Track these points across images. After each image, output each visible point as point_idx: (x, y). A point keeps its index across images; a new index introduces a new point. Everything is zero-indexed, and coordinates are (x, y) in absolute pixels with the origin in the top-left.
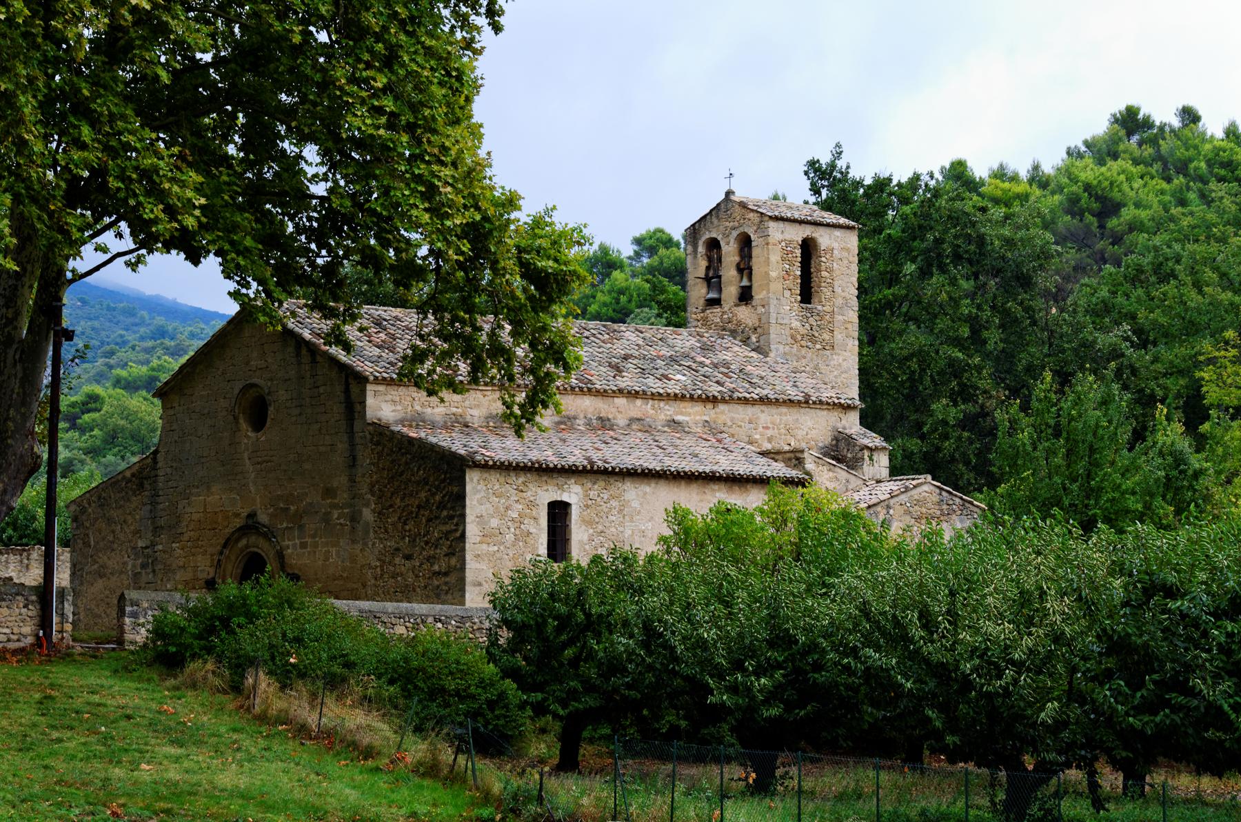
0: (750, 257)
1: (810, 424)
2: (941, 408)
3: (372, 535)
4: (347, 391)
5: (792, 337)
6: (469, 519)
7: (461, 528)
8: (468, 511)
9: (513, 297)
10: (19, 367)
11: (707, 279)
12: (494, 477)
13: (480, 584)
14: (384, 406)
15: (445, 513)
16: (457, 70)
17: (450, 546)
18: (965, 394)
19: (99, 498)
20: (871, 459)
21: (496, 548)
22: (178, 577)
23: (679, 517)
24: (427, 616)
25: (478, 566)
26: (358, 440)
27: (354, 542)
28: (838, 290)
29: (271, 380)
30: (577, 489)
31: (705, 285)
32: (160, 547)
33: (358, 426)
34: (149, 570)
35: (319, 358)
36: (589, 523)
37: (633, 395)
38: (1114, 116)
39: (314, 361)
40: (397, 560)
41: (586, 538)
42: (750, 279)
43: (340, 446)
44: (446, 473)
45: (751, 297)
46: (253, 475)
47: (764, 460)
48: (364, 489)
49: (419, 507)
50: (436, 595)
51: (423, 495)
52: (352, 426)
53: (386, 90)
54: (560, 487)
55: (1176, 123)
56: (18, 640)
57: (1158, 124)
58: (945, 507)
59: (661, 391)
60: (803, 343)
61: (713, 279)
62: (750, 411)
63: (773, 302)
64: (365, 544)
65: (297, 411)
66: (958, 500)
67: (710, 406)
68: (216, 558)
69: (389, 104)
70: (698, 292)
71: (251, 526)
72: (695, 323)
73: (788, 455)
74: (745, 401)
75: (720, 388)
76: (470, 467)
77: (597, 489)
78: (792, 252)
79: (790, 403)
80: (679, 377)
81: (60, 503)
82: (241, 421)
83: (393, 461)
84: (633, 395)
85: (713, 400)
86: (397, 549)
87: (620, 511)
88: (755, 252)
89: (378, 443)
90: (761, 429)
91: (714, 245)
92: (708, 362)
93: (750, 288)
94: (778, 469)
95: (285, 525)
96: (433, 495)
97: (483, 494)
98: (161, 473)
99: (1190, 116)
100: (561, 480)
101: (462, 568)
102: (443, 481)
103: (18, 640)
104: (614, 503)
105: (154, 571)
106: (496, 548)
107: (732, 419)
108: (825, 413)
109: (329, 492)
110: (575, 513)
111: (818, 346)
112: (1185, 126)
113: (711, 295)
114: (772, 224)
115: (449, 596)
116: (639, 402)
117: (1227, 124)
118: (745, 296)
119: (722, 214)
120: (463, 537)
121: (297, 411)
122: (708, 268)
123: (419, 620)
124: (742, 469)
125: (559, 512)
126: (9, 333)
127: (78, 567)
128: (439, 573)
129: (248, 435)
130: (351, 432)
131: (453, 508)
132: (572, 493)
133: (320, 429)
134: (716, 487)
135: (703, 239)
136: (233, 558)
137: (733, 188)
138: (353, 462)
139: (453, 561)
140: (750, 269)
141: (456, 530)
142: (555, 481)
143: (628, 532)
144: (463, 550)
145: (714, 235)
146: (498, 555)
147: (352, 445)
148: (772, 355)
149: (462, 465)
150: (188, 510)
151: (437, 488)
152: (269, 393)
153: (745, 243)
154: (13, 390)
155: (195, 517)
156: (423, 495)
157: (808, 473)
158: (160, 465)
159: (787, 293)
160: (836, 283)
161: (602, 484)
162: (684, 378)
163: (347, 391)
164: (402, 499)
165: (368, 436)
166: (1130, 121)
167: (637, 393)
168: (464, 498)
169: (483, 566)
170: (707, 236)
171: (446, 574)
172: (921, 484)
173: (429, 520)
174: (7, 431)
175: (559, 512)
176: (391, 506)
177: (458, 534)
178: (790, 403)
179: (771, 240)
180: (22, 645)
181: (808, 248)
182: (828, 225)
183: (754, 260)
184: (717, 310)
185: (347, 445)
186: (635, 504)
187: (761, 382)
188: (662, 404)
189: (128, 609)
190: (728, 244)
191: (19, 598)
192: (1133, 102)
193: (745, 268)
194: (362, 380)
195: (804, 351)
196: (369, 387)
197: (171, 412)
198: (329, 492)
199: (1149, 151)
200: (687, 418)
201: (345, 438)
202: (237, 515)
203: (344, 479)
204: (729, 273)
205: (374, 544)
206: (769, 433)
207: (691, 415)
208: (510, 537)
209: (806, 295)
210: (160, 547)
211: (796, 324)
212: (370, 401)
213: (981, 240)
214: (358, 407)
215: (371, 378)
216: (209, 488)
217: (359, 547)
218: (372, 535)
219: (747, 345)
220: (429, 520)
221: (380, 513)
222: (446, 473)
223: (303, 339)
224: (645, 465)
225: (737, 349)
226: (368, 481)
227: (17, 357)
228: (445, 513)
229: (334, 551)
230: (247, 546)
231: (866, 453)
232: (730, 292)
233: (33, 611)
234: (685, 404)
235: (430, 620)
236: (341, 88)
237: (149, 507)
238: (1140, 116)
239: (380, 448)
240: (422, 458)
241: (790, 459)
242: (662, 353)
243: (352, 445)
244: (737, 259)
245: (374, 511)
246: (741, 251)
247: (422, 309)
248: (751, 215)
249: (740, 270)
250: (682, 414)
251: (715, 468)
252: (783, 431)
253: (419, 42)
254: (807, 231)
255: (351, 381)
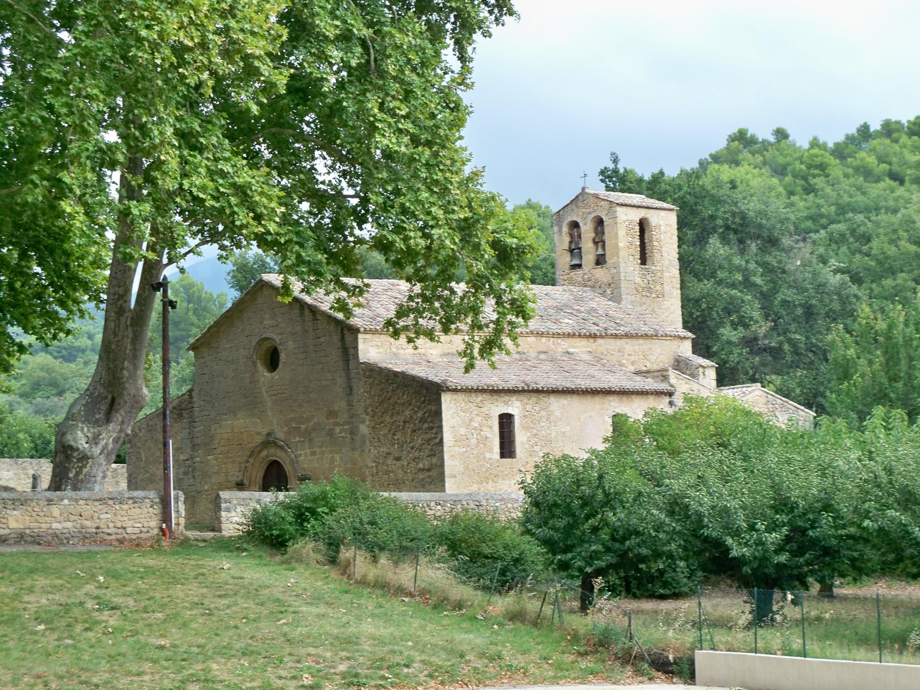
0: (603, 233)
2: (728, 333)
3: (368, 443)
4: (343, 339)
5: (636, 289)
6: (445, 429)
7: (439, 436)
8: (444, 423)
9: (479, 265)
10: (130, 330)
11: (571, 251)
12: (460, 397)
13: (455, 477)
14: (371, 349)
15: (426, 425)
16: (454, 102)
17: (432, 450)
18: (743, 322)
19: (148, 425)
20: (704, 375)
21: (464, 450)
22: (213, 481)
23: (619, 422)
24: (430, 501)
25: (453, 463)
26: (353, 375)
27: (353, 449)
28: (665, 254)
29: (281, 334)
30: (517, 404)
31: (569, 254)
32: (198, 459)
33: (352, 364)
34: (190, 476)
35: (319, 317)
36: (526, 428)
37: (540, 334)
38: (730, 136)
39: (315, 319)
40: (389, 462)
41: (525, 439)
42: (604, 248)
43: (339, 380)
44: (425, 396)
45: (605, 262)
46: (270, 404)
47: (638, 378)
48: (360, 410)
49: (405, 422)
50: (422, 486)
51: (407, 413)
52: (348, 365)
53: (406, 117)
54: (506, 403)
55: (772, 139)
56: (148, 532)
57: (760, 140)
58: (771, 406)
59: (559, 331)
60: (644, 293)
61: (575, 250)
63: (622, 265)
64: (363, 451)
65: (303, 356)
66: (779, 401)
67: (591, 340)
68: (243, 465)
69: (409, 126)
70: (564, 260)
71: (269, 442)
72: (563, 282)
73: (656, 374)
74: (616, 336)
75: (597, 328)
76: (444, 391)
77: (531, 402)
78: (633, 229)
79: (646, 336)
80: (567, 321)
82: (259, 365)
83: (382, 389)
84: (540, 334)
85: (594, 336)
86: (389, 454)
87: (548, 419)
88: (606, 230)
89: (369, 377)
91: (575, 225)
92: (582, 309)
93: (604, 255)
94: (650, 384)
95: (297, 439)
96: (416, 412)
97: (454, 410)
98: (196, 405)
99: (781, 134)
100: (506, 398)
101: (442, 465)
102: (424, 402)
103: (148, 532)
104: (543, 413)
105: (194, 477)
106: (464, 450)
107: (607, 350)
108: (668, 342)
109: (332, 414)
110: (517, 421)
111: (654, 295)
112: (779, 141)
113: (574, 262)
114: (619, 209)
115: (432, 486)
116: (544, 340)
117: (811, 139)
118: (600, 261)
119: (580, 204)
120: (441, 442)
121: (303, 356)
122: (571, 242)
123: (425, 505)
124: (628, 385)
125: (506, 421)
126: (121, 306)
127: (133, 476)
128: (423, 470)
129: (264, 375)
130: (347, 370)
131: (432, 422)
132: (514, 407)
133: (322, 369)
135: (566, 222)
136: (257, 465)
137: (587, 185)
138: (350, 390)
139: (434, 460)
140: (604, 242)
141: (436, 438)
142: (502, 399)
143: (554, 434)
144: (442, 451)
145: (575, 219)
146: (466, 454)
147: (349, 379)
148: (623, 302)
149: (437, 391)
150: (219, 431)
151: (419, 407)
152: (280, 344)
153: (599, 223)
154: (126, 348)
155: (225, 436)
156: (407, 413)
157: (672, 386)
158: (195, 399)
159: (631, 258)
160: (664, 250)
161: (534, 399)
162: (571, 322)
163: (343, 339)
164: (391, 417)
165: (362, 372)
166: (742, 138)
167: (543, 333)
168: (441, 414)
169: (457, 463)
170: (570, 219)
171: (429, 470)
172: (754, 390)
173: (414, 431)
174: (122, 378)
175: (506, 421)
176: (382, 422)
177: (437, 440)
178: (646, 336)
179: (619, 220)
180: (150, 534)
181: (643, 225)
182: (656, 209)
183: (606, 235)
184: (579, 272)
185: (344, 379)
186: (558, 414)
187: (623, 323)
188: (559, 341)
189: (223, 505)
190: (585, 224)
191: (147, 500)
192: (743, 126)
193: (599, 241)
194: (355, 331)
195: (644, 299)
196: (360, 336)
197: (202, 361)
198: (332, 414)
199: (759, 159)
200: (577, 350)
201: (343, 373)
202: (259, 434)
203: (343, 404)
204: (587, 245)
205: (370, 450)
206: (632, 358)
207: (580, 347)
208: (474, 441)
209: (644, 260)
210: (198, 459)
211: (638, 280)
212: (361, 346)
213: (743, 216)
214: (352, 351)
215: (362, 330)
216: (235, 415)
217: (357, 453)
218: (368, 443)
219: (604, 296)
220: (414, 431)
221: (373, 428)
222: (425, 396)
223: (306, 303)
224: (564, 384)
225: (598, 299)
226: (363, 404)
227: (129, 322)
228: (426, 425)
229: (337, 457)
230: (268, 456)
231: (701, 370)
232: (589, 257)
233: (157, 509)
235: (433, 504)
236: (374, 116)
237: (187, 431)
238: (749, 135)
239: (371, 380)
240: (406, 386)
241: (658, 376)
242: (550, 304)
243: (349, 379)
244: (593, 235)
245: (368, 426)
246: (596, 229)
247: (409, 280)
248: (603, 203)
249: (595, 243)
250: (573, 347)
251: (610, 385)
252: (641, 357)
253: (427, 81)
254: (642, 213)
255: (345, 332)
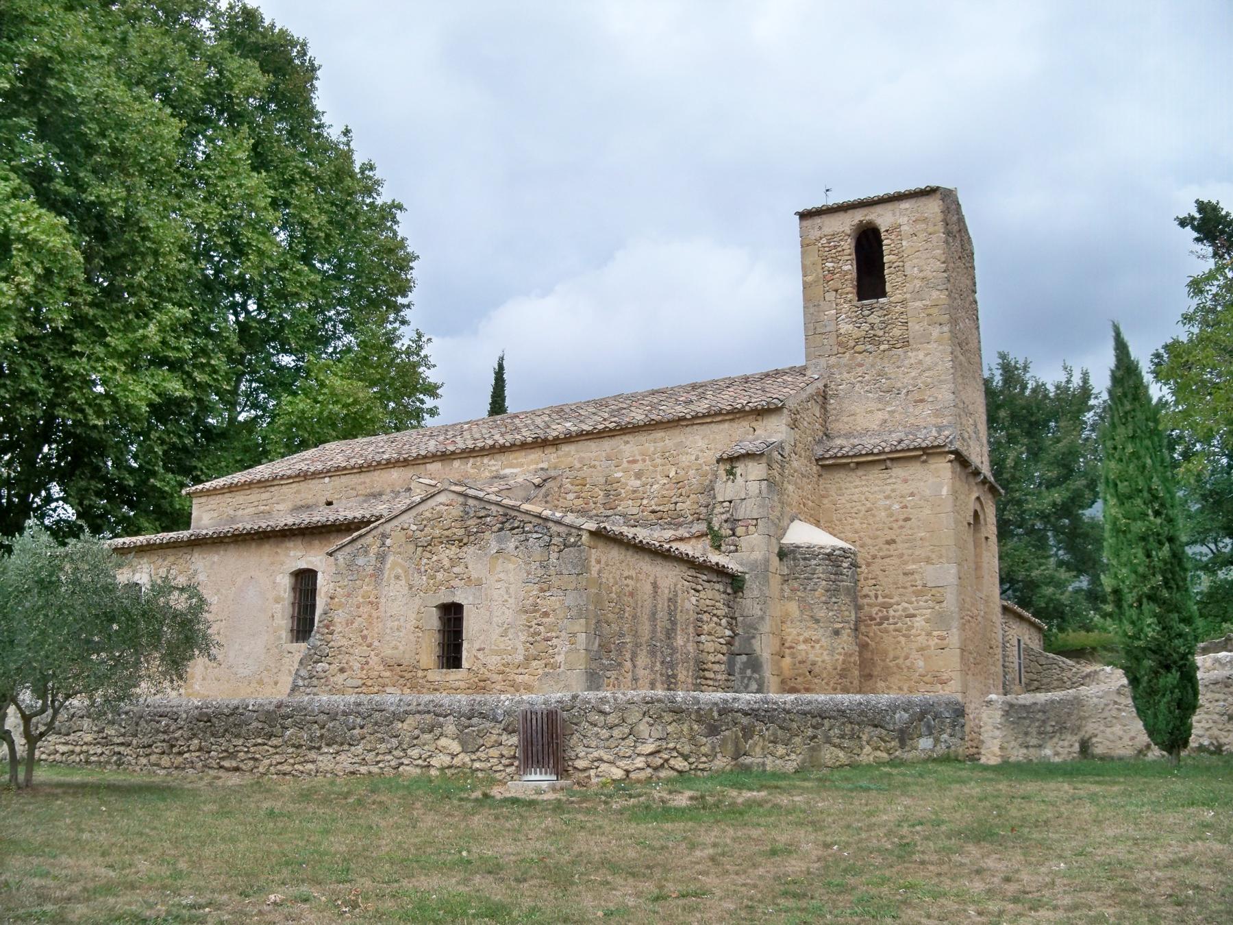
1: (701, 444)
62: (607, 445)
81: (1018, 755)
85: (556, 442)
90: (625, 465)
108: (726, 425)
116: (456, 464)
125: (305, 581)
134: (291, 544)
175: (305, 581)
188: (486, 460)
206: (637, 467)
234: (377, 473)
